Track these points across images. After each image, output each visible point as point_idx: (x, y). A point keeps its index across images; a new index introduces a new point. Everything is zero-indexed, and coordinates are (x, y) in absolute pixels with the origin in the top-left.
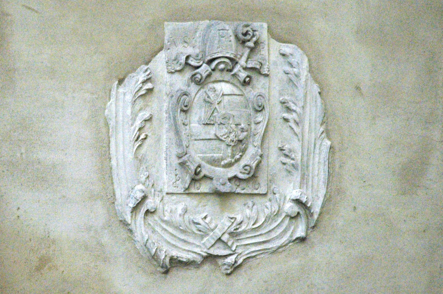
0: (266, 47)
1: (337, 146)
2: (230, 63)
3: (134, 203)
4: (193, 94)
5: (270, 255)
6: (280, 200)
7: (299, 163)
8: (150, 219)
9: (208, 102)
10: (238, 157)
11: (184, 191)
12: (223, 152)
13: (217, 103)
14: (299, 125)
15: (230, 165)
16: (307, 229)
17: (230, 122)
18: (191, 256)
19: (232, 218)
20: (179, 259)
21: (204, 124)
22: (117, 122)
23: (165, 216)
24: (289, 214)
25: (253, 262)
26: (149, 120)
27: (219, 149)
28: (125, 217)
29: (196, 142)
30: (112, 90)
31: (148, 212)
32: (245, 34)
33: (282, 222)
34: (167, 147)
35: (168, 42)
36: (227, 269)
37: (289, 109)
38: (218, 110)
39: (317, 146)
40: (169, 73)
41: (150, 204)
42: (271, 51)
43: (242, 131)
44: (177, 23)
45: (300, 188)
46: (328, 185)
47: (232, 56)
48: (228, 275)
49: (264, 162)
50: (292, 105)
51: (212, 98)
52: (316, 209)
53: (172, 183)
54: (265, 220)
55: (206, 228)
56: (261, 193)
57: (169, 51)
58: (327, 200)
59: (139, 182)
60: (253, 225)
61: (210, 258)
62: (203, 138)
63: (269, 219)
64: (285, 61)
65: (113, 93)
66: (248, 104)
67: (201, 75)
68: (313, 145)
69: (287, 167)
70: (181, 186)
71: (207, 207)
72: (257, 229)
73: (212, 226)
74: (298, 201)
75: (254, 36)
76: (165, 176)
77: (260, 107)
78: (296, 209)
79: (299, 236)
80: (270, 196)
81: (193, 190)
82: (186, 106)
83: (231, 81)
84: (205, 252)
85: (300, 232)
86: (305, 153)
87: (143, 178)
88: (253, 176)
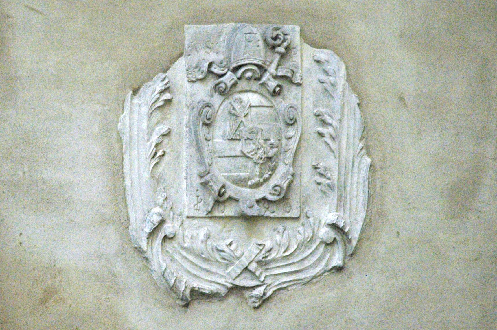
0: (298, 53)
1: (378, 164)
2: (258, 71)
3: (150, 228)
4: (217, 106)
5: (303, 287)
6: (314, 224)
7: (336, 182)
8: (168, 246)
9: (233, 115)
10: (267, 176)
11: (206, 214)
12: (250, 171)
13: (243, 115)
14: (336, 140)
15: (258, 185)
16: (345, 258)
17: (258, 137)
18: (214, 288)
19: (260, 245)
20: (201, 290)
21: (229, 139)
22: (131, 137)
23: (185, 243)
24: (325, 240)
25: (284, 295)
26: (168, 134)
27: (246, 167)
28: (141, 243)
29: (219, 159)
30: (126, 101)
31: (166, 238)
32: (275, 38)
33: (316, 249)
34: (187, 165)
35: (189, 47)
36: (255, 302)
37: (324, 123)
38: (245, 123)
39: (356, 164)
40: (190, 82)
41: (168, 229)
42: (305, 58)
43: (272, 148)
44: (199, 26)
45: (337, 211)
46: (368, 208)
47: (260, 63)
48: (256, 308)
49: (296, 182)
50: (328, 117)
51: (237, 110)
52: (355, 235)
53: (193, 205)
54: (298, 247)
55: (231, 256)
56: (293, 216)
57: (189, 57)
58: (367, 224)
59: (156, 205)
60: (284, 252)
61: (236, 290)
62: (228, 155)
63: (301, 246)
64: (320, 69)
65: (127, 104)
66: (279, 117)
67: (225, 84)
68: (351, 163)
69: (322, 187)
70: (203, 208)
71: (232, 232)
72: (288, 257)
73: (238, 253)
74: (334, 226)
75: (284, 40)
76: (185, 198)
77: (291, 120)
78: (332, 234)
79: (336, 265)
80: (303, 220)
81: (217, 214)
82: (209, 119)
83: (259, 91)
84: (230, 283)
85: (337, 260)
86: (343, 172)
87: (161, 200)
88: (284, 198)
